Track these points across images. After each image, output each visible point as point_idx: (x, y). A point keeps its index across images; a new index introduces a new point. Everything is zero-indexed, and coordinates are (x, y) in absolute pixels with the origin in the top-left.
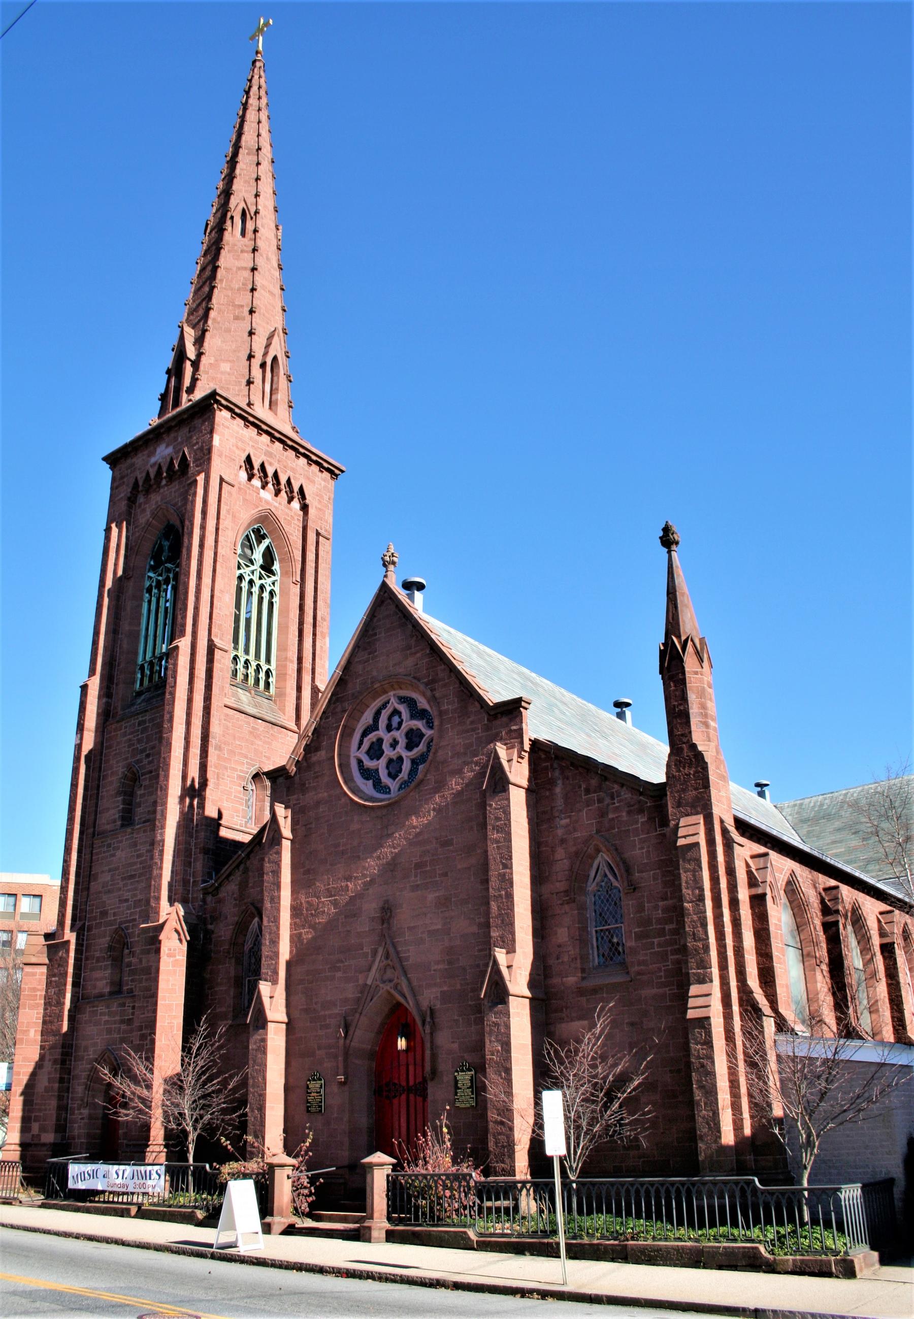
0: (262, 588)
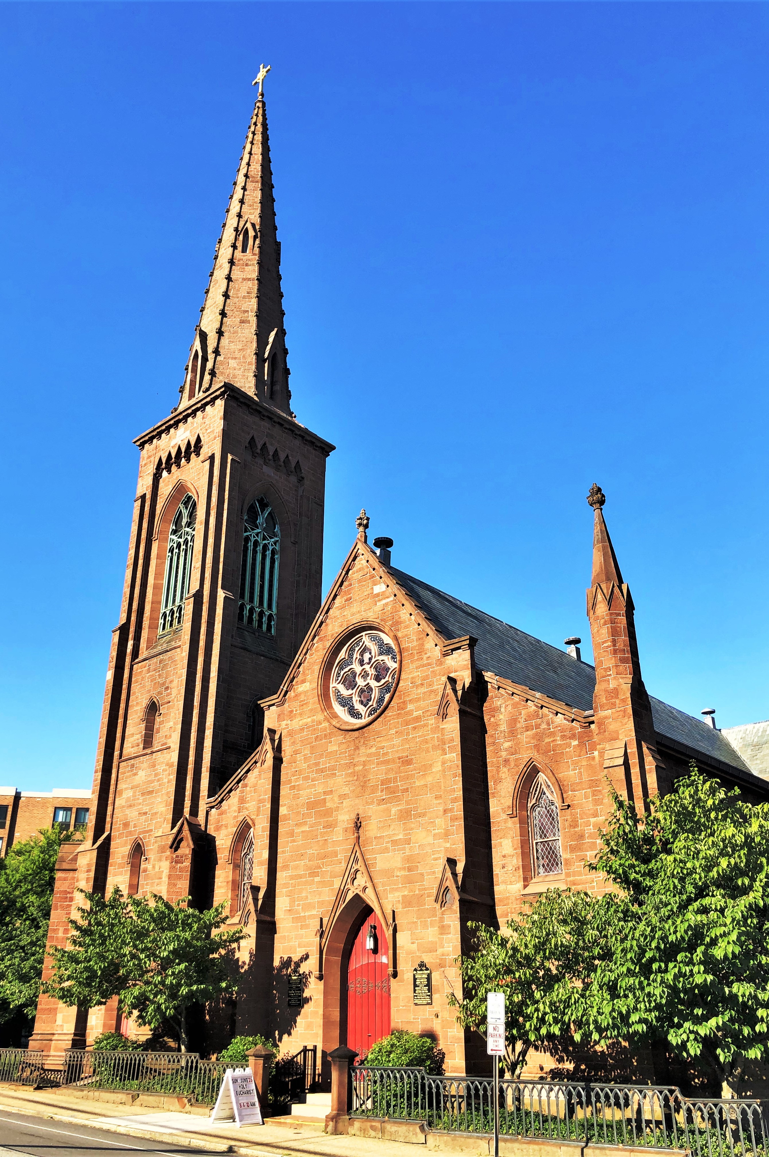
0: (265, 547)
